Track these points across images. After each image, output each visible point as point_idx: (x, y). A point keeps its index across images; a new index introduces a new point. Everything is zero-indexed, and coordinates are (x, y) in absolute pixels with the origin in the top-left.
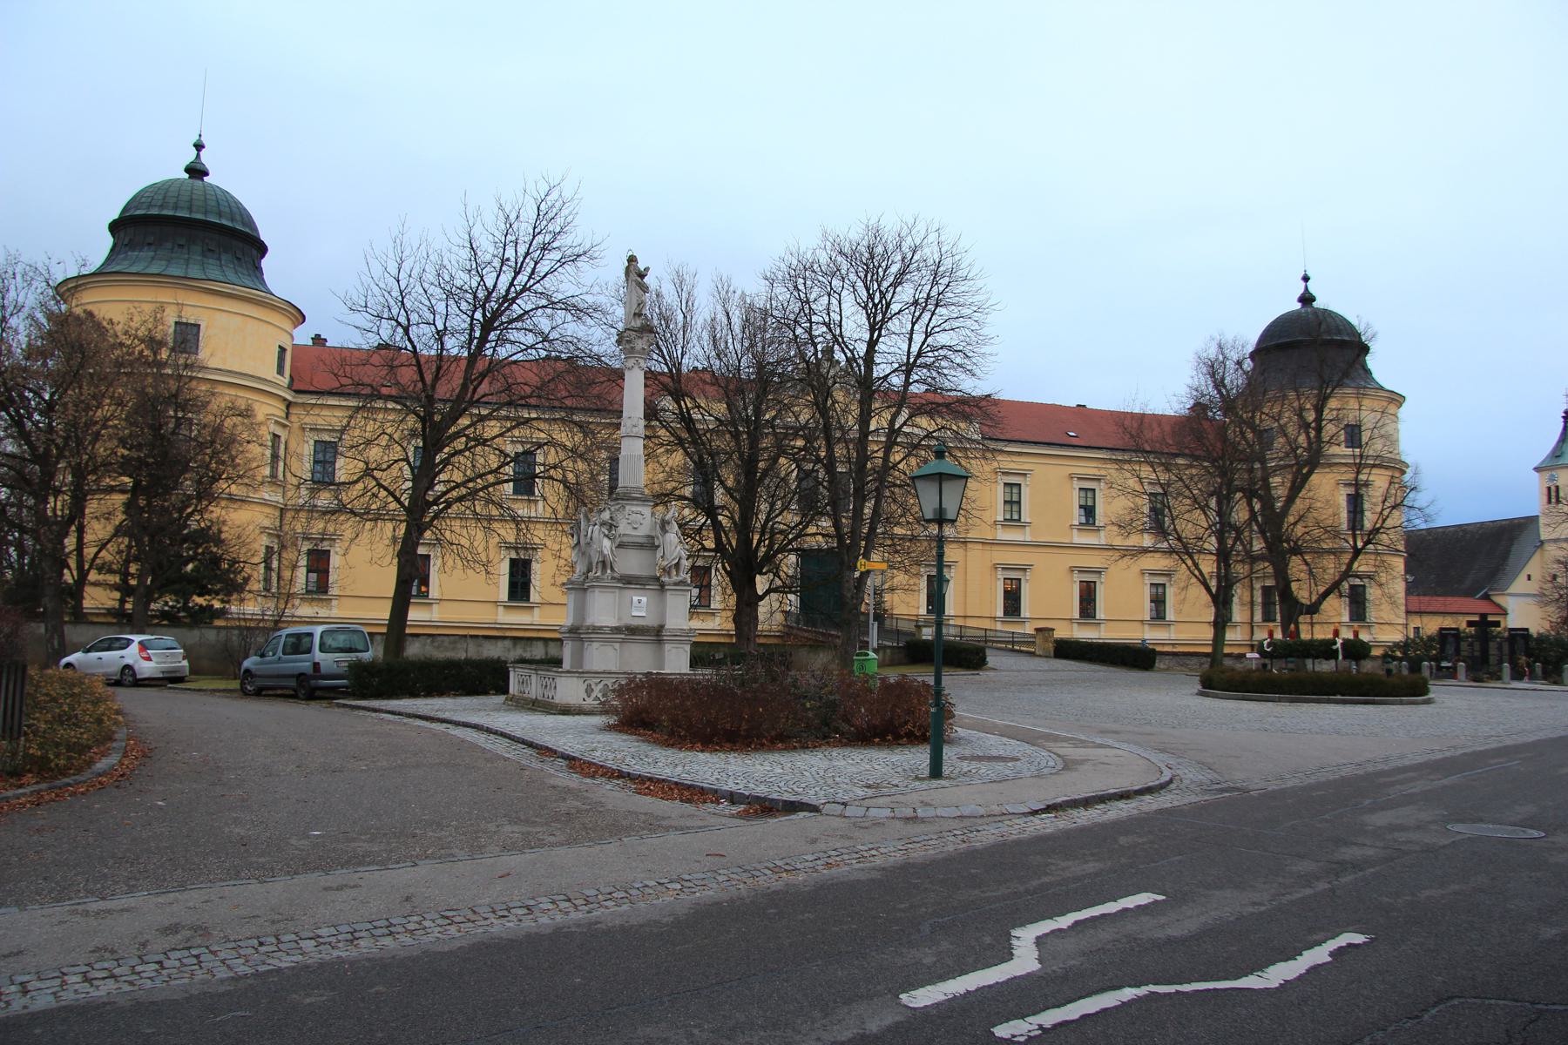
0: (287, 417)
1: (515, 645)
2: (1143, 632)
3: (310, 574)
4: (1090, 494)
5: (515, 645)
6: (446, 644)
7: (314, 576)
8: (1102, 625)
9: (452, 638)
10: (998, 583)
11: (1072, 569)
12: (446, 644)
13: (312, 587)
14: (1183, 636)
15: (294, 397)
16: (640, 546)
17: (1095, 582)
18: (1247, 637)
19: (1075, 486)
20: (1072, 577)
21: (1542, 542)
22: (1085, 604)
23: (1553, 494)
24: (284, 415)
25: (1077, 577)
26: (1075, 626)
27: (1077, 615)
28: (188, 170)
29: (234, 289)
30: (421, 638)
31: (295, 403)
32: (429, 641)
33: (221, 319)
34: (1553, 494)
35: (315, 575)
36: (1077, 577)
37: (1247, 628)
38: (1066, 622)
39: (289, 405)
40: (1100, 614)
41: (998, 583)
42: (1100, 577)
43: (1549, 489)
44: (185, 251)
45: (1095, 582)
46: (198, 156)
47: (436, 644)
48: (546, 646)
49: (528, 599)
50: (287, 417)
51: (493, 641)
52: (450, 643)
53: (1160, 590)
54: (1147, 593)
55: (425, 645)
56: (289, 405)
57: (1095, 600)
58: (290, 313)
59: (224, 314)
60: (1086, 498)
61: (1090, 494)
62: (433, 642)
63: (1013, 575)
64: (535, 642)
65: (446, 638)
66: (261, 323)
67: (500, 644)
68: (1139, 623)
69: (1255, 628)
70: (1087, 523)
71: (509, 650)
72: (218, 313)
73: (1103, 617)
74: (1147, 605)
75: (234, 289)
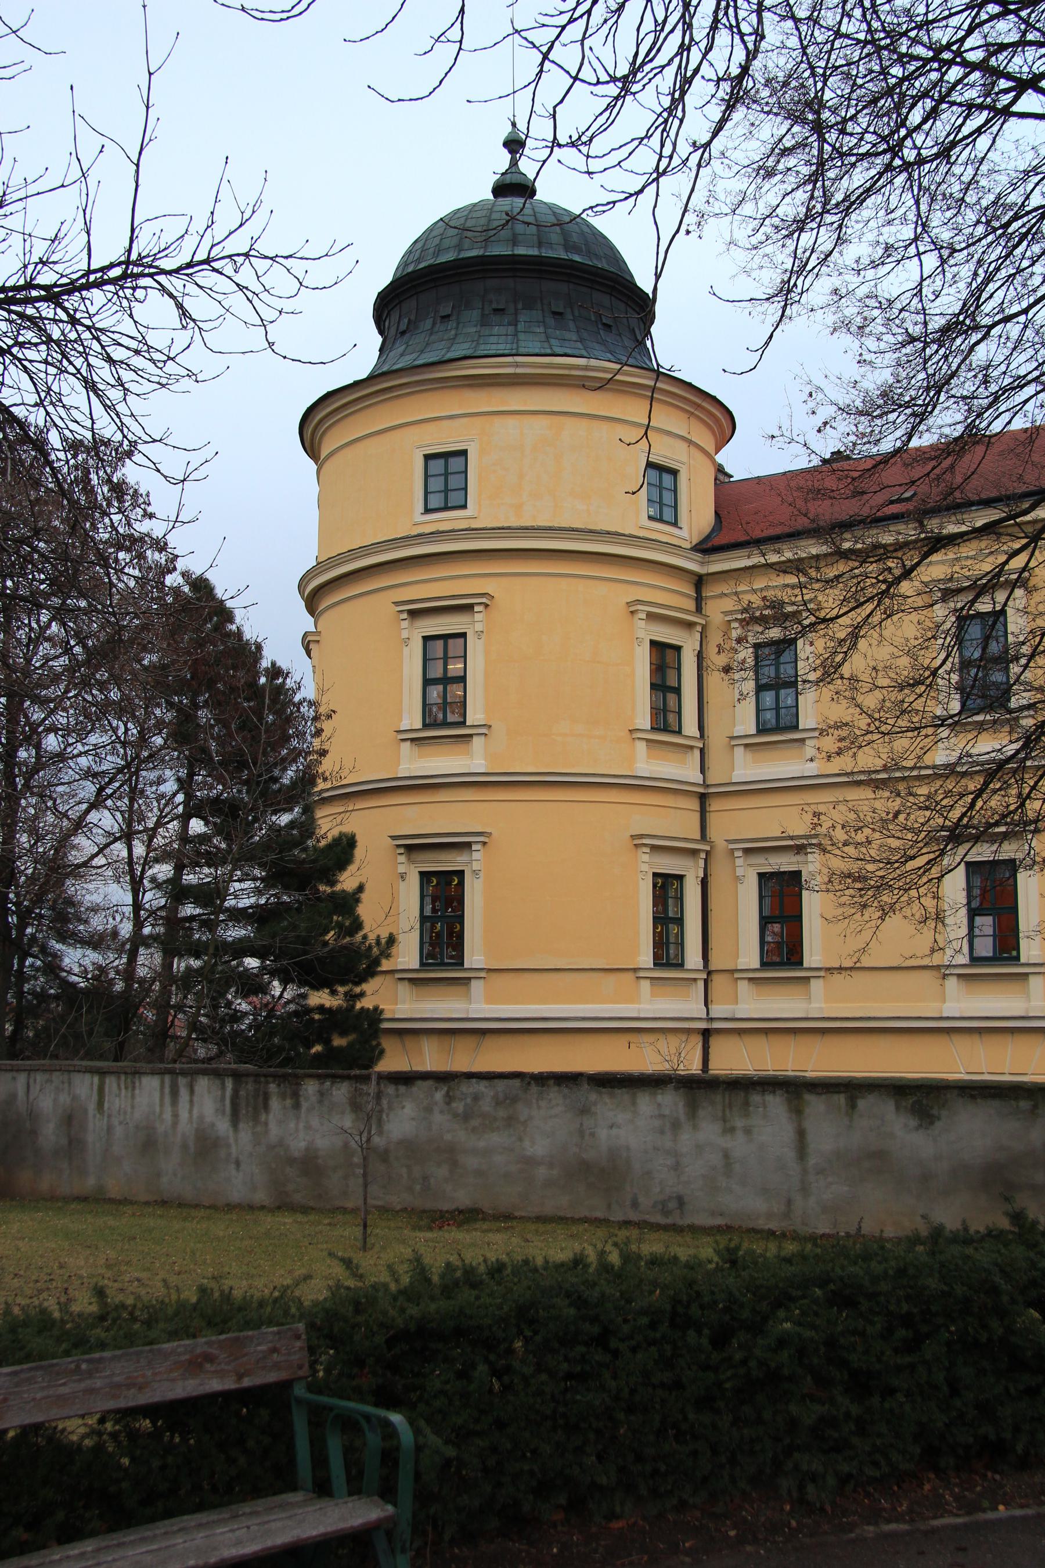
0: (699, 609)
1: (693, 1108)
3: (978, 920)
5: (693, 1108)
6: (486, 1105)
7: (985, 923)
9: (501, 1085)
12: (486, 1105)
13: (985, 947)
15: (702, 563)
24: (691, 605)
28: (500, 190)
29: (517, 365)
30: (421, 1088)
31: (708, 574)
32: (439, 1096)
33: (508, 429)
35: (988, 920)
38: (927, 975)
39: (699, 582)
44: (452, 324)
46: (514, 163)
47: (459, 1106)
48: (797, 1111)
49: (459, 961)
50: (699, 609)
51: (623, 1095)
52: (498, 1103)
55: (429, 1110)
56: (699, 582)
58: (685, 398)
59: (511, 421)
62: (449, 1099)
64: (756, 1098)
65: (482, 1087)
66: (596, 424)
67: (645, 1102)
71: (676, 1126)
72: (497, 420)
75: (517, 365)
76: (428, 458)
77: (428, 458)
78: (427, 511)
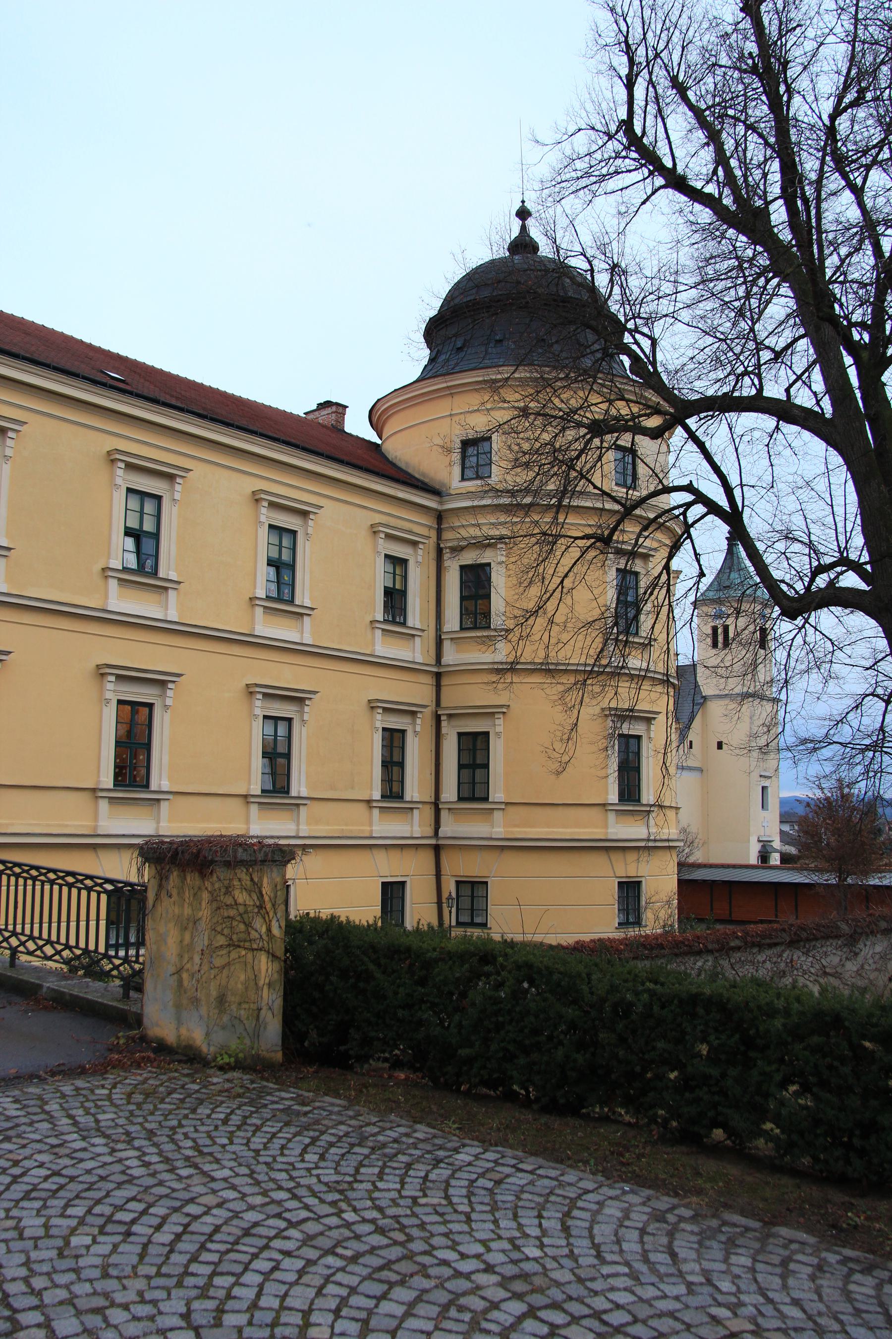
2: (606, 826)
4: (149, 507)
8: (164, 805)
10: (106, 710)
11: (101, 672)
14: (322, 829)
16: (438, 687)
17: (150, 706)
18: (429, 831)
19: (380, 548)
20: (102, 690)
21: (705, 698)
22: (127, 756)
23: (720, 639)
25: (113, 691)
26: (104, 805)
27: (107, 780)
34: (720, 639)
36: (113, 691)
37: (429, 812)
40: (160, 779)
41: (106, 710)
42: (163, 696)
43: (715, 629)
45: (150, 706)
53: (282, 730)
54: (257, 733)
57: (148, 746)
60: (142, 513)
61: (149, 507)
63: (395, 722)
68: (238, 802)
69: (444, 815)
70: (279, 599)
73: (166, 785)
74: (258, 763)
78: (463, 479)
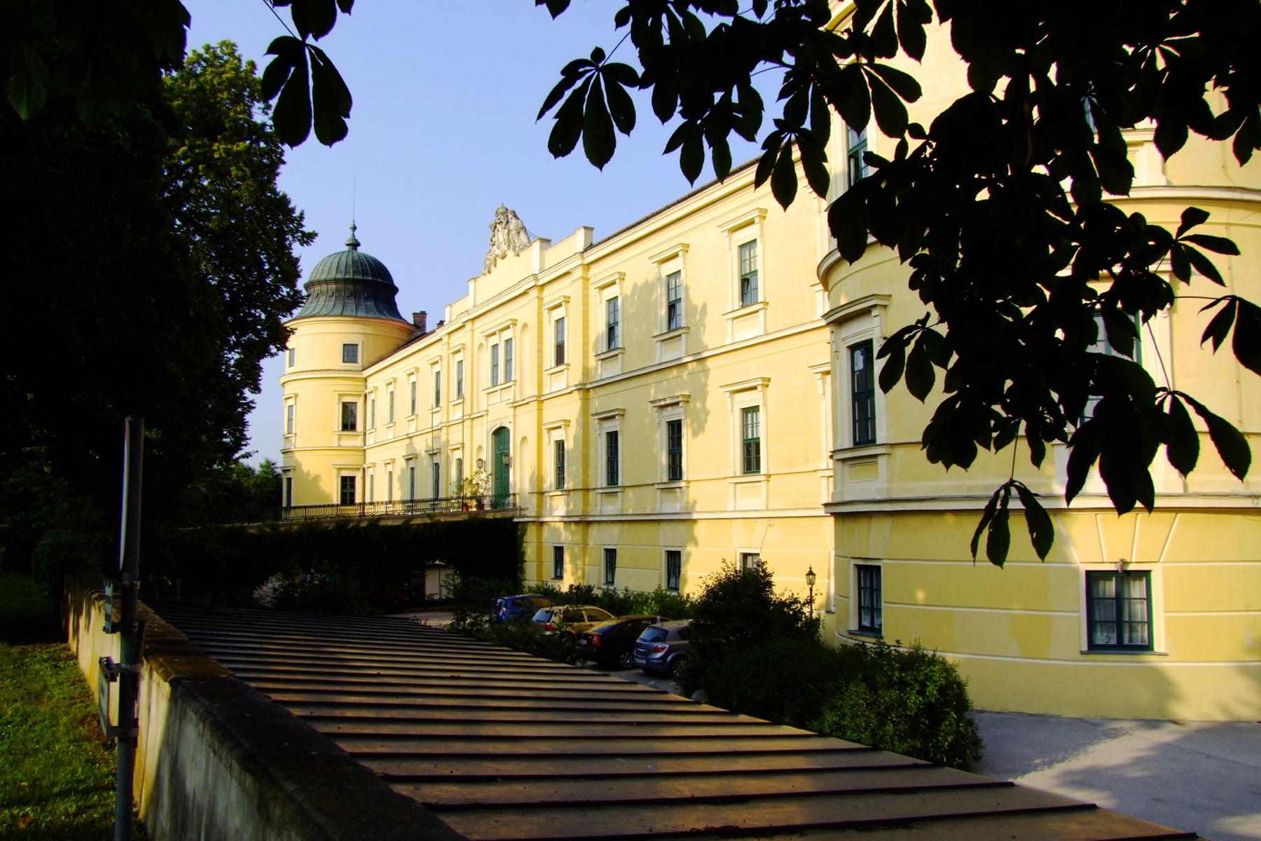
76: (344, 345)
77: (344, 345)
